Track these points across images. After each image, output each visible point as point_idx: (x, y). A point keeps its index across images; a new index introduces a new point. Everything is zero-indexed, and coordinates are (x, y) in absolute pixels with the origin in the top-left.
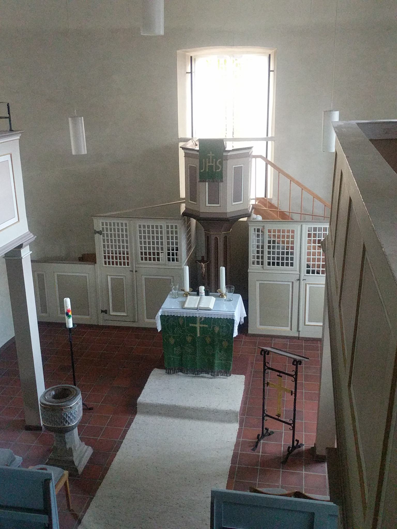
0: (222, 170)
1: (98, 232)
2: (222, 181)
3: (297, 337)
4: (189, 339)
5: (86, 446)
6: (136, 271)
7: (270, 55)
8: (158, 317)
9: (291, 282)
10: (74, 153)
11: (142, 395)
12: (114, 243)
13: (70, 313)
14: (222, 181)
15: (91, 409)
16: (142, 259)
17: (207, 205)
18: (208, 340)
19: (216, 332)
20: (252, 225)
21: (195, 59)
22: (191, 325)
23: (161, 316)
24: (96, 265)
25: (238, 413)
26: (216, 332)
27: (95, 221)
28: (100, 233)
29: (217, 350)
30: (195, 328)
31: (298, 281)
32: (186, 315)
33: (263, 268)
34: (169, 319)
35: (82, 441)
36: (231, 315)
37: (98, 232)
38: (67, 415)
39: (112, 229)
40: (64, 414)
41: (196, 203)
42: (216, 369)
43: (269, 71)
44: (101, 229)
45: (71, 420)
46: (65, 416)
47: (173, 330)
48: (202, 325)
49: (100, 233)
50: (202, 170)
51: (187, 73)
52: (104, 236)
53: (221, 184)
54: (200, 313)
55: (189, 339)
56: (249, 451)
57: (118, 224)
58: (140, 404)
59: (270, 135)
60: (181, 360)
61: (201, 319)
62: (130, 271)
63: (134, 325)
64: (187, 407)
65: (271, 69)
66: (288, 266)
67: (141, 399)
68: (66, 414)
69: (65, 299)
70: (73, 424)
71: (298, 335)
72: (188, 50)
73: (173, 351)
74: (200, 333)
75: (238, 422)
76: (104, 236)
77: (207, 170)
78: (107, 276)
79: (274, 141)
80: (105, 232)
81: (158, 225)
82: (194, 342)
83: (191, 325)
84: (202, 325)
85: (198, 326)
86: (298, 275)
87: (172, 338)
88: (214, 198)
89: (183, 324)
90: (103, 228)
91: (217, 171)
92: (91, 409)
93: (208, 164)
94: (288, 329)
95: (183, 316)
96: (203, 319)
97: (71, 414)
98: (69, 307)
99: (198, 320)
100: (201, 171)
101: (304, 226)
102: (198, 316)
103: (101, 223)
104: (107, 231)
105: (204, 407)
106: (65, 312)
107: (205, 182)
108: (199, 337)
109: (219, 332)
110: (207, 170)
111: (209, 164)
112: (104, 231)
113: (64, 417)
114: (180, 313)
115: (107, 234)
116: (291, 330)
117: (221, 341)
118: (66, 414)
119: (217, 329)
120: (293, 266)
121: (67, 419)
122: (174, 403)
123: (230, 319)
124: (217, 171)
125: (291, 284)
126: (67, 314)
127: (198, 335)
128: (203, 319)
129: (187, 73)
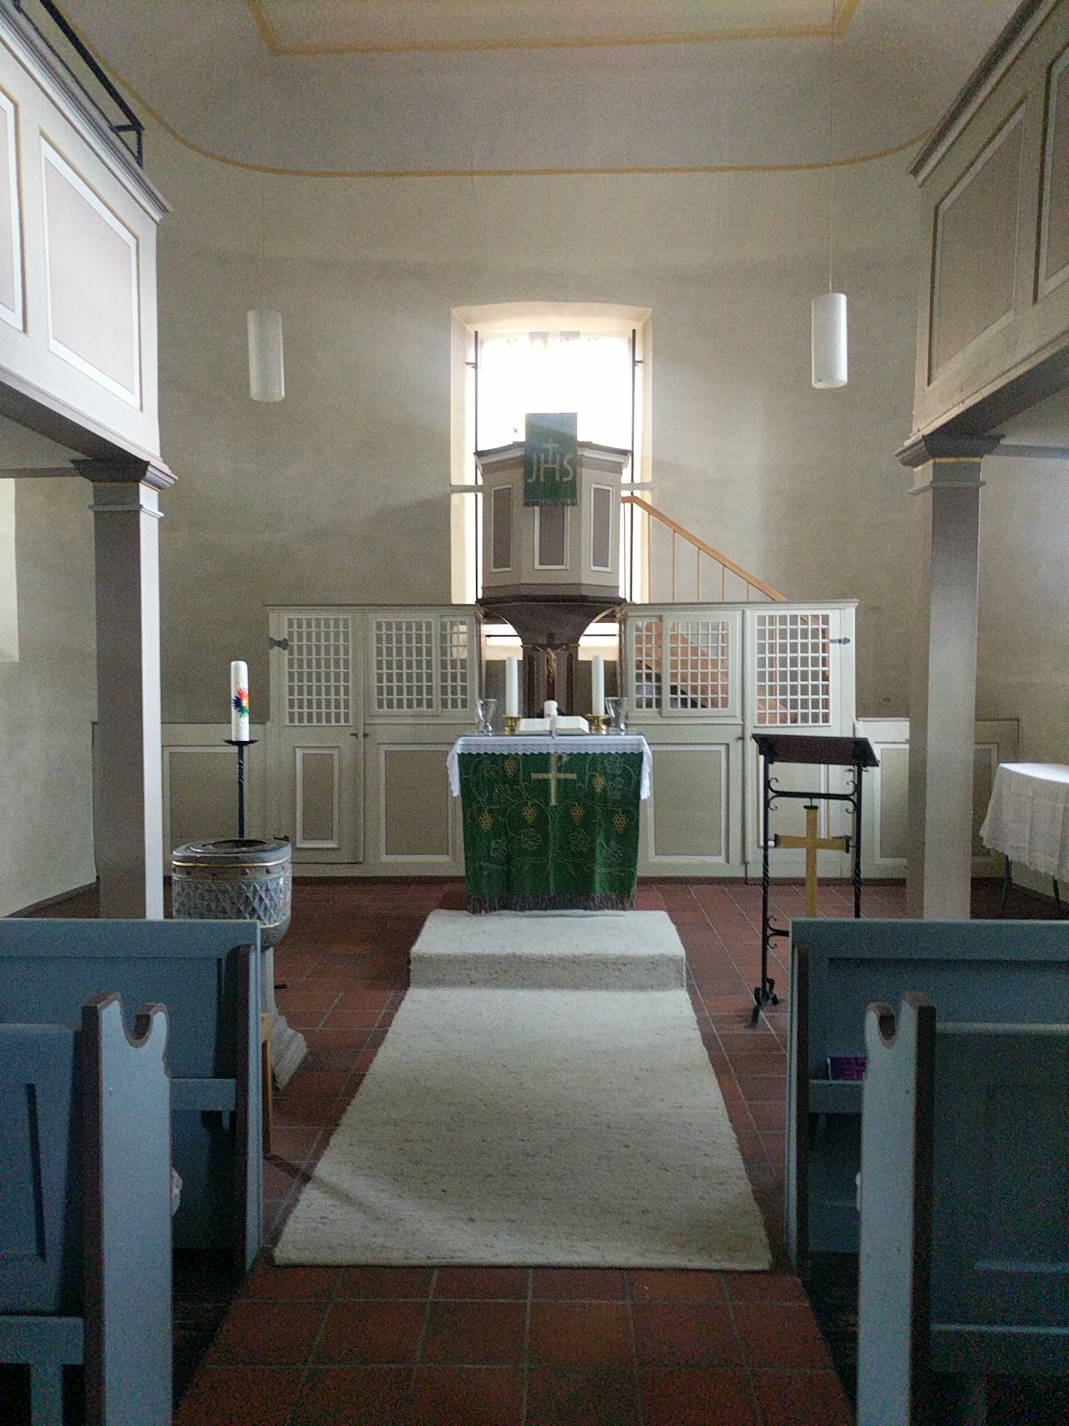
0: (574, 477)
1: (279, 644)
2: (574, 504)
3: (742, 878)
4: (529, 814)
5: (290, 1032)
6: (365, 735)
7: (634, 331)
8: (453, 757)
9: (724, 744)
10: (254, 390)
11: (420, 939)
12: (314, 669)
13: (245, 703)
14: (574, 504)
15: (284, 987)
16: (380, 706)
17: (537, 566)
18: (578, 813)
19: (598, 790)
20: (635, 614)
21: (482, 342)
22: (534, 776)
23: (461, 757)
24: (269, 724)
25: (682, 960)
26: (598, 790)
27: (273, 617)
28: (283, 644)
29: (600, 840)
30: (546, 782)
31: (741, 741)
32: (524, 749)
33: (660, 713)
34: (480, 763)
35: (280, 1014)
36: (633, 745)
37: (279, 644)
38: (255, 891)
39: (296, 688)
40: (248, 886)
41: (509, 569)
42: (598, 889)
43: (634, 362)
44: (286, 637)
45: (266, 909)
46: (250, 895)
47: (491, 791)
48: (562, 776)
49: (283, 644)
50: (531, 478)
51: (468, 364)
52: (291, 653)
53: (569, 510)
54: (558, 745)
55: (529, 814)
56: (740, 1029)
57: (327, 621)
58: (421, 959)
59: (636, 481)
60: (508, 873)
61: (560, 757)
62: (352, 735)
63: (356, 872)
64: (546, 956)
65: (637, 359)
66: (717, 707)
67: (419, 948)
68: (252, 887)
69: (233, 664)
70: (270, 923)
71: (742, 874)
72: (475, 310)
73: (488, 848)
74: (557, 799)
75: (683, 986)
76: (291, 653)
77: (542, 479)
78: (295, 750)
79: (651, 490)
80: (296, 642)
81: (421, 622)
82: (542, 817)
83: (534, 776)
84: (562, 776)
85: (552, 776)
86: (740, 728)
87: (486, 815)
88: (553, 551)
89: (516, 775)
90: (290, 634)
91: (564, 479)
92: (284, 987)
93: (543, 466)
94: (721, 860)
95: (517, 754)
96: (565, 759)
97: (267, 890)
98: (244, 684)
99: (553, 761)
100: (530, 481)
101: (748, 613)
102: (552, 752)
103: (286, 622)
104: (300, 639)
105: (590, 955)
106: (233, 697)
107: (533, 505)
108: (555, 806)
109: (604, 790)
110: (542, 479)
111: (547, 466)
112: (293, 641)
113: (247, 897)
114: (508, 745)
115: (300, 648)
116: (728, 862)
117: (609, 815)
118: (252, 887)
119: (600, 783)
120: (727, 707)
121: (256, 904)
122: (509, 950)
123: (632, 753)
124: (564, 479)
125: (723, 749)
126: (238, 703)
127: (553, 802)
128: (565, 759)
129: (468, 364)
